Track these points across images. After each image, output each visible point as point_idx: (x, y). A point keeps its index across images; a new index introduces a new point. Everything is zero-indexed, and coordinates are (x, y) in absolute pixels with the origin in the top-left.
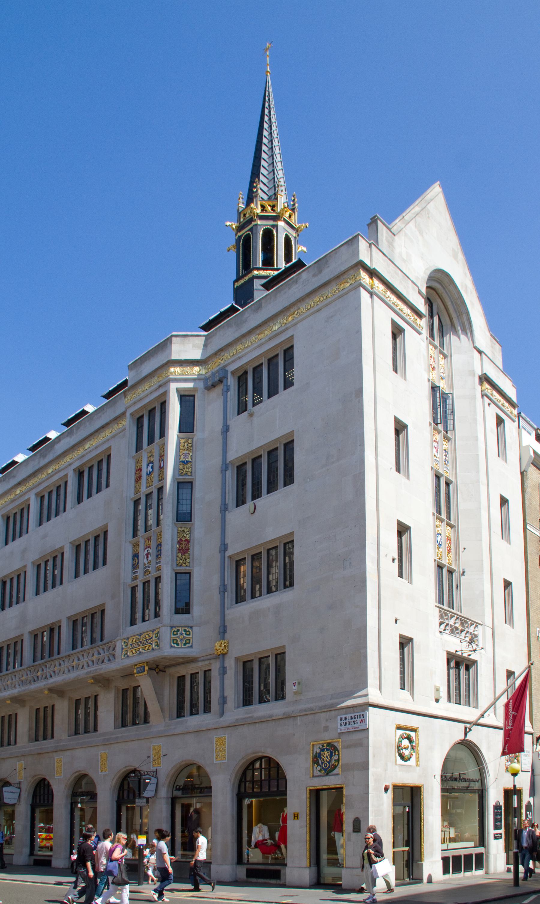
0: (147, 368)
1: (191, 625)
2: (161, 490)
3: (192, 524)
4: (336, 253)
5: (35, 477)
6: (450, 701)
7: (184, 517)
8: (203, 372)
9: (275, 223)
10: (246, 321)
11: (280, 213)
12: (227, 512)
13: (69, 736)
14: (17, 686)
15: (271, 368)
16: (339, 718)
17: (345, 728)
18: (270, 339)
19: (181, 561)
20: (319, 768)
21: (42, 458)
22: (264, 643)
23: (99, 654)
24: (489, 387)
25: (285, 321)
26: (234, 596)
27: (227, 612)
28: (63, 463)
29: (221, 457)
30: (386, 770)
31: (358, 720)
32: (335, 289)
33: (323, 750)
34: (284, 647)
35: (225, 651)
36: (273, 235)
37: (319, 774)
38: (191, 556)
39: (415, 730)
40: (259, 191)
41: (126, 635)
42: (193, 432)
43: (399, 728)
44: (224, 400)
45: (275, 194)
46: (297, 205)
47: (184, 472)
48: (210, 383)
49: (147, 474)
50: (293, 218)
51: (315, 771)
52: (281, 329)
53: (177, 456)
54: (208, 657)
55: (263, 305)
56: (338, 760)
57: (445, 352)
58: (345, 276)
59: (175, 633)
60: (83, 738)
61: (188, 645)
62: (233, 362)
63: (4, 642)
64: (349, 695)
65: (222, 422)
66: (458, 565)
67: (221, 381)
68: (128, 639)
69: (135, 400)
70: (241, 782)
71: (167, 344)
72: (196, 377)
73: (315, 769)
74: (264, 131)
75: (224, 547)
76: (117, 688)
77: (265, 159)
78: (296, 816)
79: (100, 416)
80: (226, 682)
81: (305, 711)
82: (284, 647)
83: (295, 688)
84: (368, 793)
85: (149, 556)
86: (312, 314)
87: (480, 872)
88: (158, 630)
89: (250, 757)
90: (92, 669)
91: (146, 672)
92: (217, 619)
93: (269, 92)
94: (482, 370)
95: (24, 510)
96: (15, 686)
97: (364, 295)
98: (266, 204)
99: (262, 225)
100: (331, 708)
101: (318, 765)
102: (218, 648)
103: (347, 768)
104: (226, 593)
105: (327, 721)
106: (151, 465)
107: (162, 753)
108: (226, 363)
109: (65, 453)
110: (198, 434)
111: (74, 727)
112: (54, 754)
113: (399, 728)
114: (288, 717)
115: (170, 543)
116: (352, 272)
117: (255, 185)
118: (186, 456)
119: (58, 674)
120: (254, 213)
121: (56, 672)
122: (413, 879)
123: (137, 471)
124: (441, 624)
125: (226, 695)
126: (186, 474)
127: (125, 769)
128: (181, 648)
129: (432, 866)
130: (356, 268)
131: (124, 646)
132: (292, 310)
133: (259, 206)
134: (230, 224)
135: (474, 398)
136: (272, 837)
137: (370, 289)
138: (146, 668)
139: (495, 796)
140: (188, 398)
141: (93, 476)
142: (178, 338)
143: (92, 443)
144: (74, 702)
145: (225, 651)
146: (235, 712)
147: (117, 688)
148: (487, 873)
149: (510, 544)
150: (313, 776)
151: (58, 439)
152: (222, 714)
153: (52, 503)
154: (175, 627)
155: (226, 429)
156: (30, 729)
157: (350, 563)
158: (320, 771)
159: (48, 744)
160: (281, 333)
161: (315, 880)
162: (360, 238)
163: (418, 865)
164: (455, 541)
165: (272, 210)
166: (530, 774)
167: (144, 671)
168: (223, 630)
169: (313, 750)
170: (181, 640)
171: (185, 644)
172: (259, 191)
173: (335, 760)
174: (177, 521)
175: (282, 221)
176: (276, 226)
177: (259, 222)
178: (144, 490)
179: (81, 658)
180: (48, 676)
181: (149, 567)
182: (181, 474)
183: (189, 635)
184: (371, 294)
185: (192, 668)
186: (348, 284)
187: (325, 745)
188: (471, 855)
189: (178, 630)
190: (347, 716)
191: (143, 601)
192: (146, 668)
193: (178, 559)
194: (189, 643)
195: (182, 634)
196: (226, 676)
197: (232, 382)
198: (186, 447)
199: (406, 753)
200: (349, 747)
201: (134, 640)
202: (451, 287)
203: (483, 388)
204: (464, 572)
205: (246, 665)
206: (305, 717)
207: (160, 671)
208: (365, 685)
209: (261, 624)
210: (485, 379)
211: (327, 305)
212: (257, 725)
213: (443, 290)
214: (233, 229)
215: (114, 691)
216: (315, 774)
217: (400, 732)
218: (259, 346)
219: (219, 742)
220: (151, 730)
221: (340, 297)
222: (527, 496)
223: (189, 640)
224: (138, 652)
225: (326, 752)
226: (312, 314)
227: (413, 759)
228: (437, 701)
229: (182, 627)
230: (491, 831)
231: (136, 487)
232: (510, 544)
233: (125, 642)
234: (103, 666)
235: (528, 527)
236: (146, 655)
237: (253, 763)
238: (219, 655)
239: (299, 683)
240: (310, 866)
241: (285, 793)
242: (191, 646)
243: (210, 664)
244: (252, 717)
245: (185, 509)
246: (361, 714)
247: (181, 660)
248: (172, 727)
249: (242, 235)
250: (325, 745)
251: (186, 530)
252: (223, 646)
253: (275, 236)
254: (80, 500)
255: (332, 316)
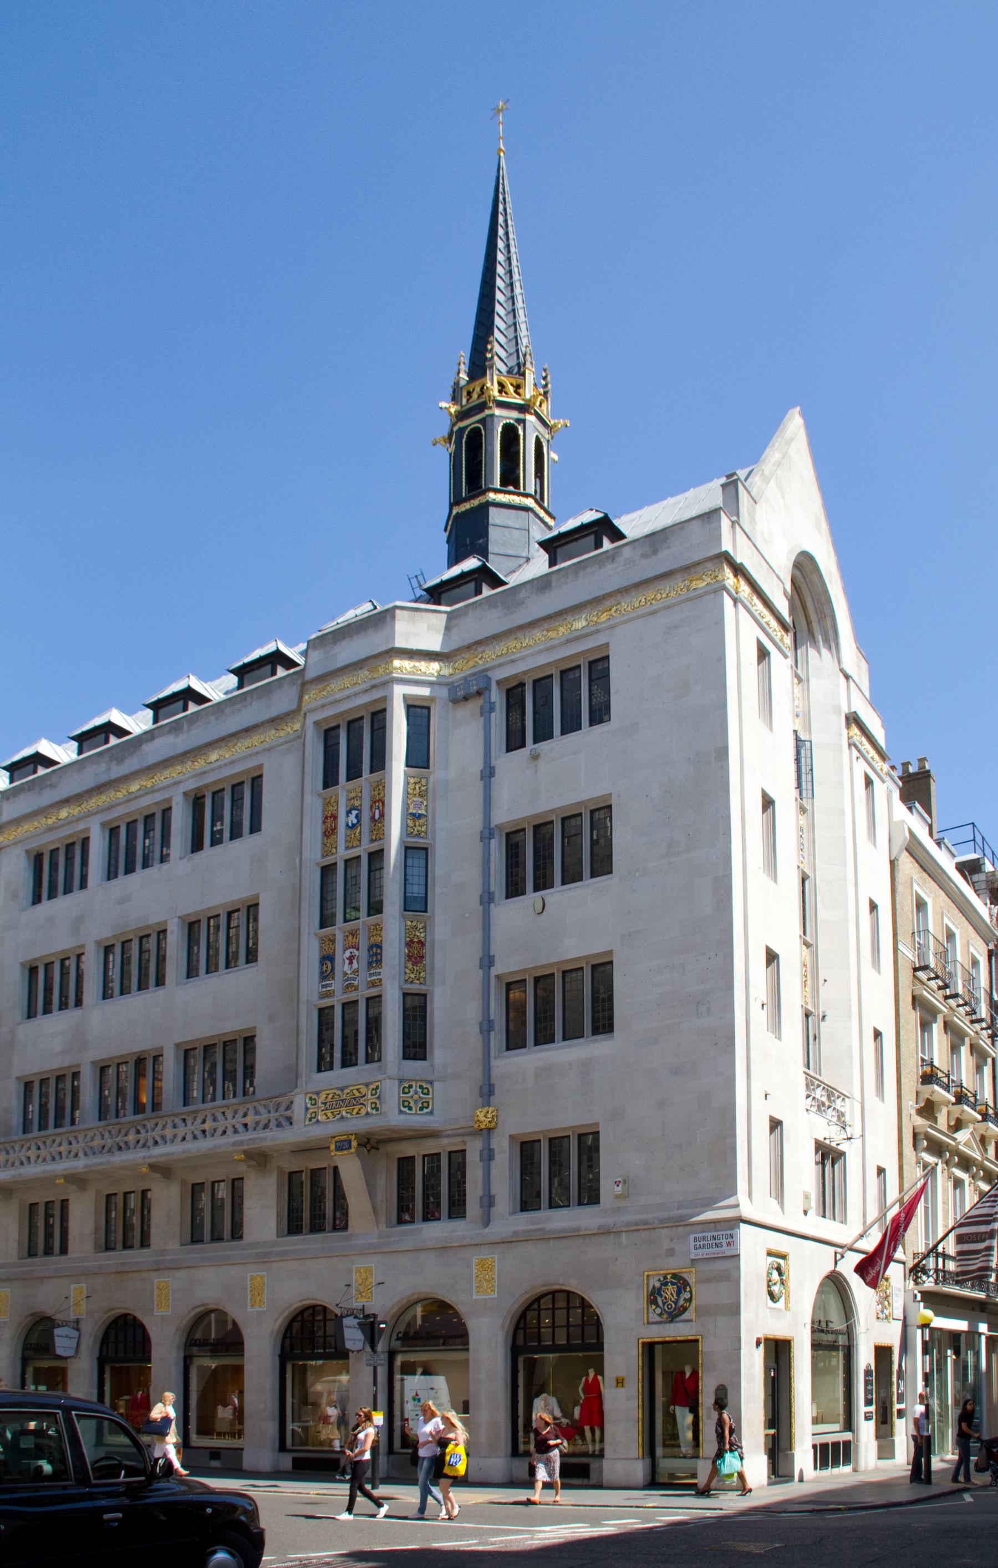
0: (348, 652)
1: (431, 1078)
2: (377, 857)
3: (430, 917)
4: (682, 529)
5: (101, 793)
6: (824, 1216)
7: (416, 904)
8: (446, 671)
9: (521, 416)
10: (523, 603)
11: (530, 400)
12: (492, 905)
13: (182, 1245)
14: (81, 1154)
15: (565, 685)
16: (692, 1237)
17: (702, 1253)
18: (568, 641)
19: (413, 976)
20: (658, 1311)
21: (114, 763)
22: (566, 1117)
23: (257, 1113)
24: (859, 733)
25: (595, 619)
26: (504, 1038)
27: (494, 1063)
28: (162, 778)
29: (481, 816)
30: (757, 1316)
31: (724, 1242)
32: (681, 585)
33: (666, 1284)
34: (597, 1124)
35: (493, 1124)
36: (518, 436)
37: (658, 1319)
38: (428, 968)
39: (784, 1257)
40: (496, 358)
41: (313, 1087)
42: (428, 767)
43: (770, 1254)
44: (485, 725)
45: (519, 365)
46: (550, 386)
47: (415, 832)
48: (461, 693)
49: (347, 825)
50: (544, 406)
51: (651, 1315)
52: (588, 630)
53: (406, 806)
54: (459, 1131)
55: (554, 584)
56: (690, 1300)
57: (799, 672)
58: (699, 569)
59: (406, 1090)
60: (210, 1249)
61: (425, 1110)
62: (500, 665)
63: (34, 1074)
64: (709, 1203)
65: (482, 759)
66: (816, 1005)
67: (479, 693)
68: (318, 1093)
69: (323, 701)
70: (517, 1328)
71: (385, 618)
72: (434, 679)
73: (651, 1310)
74: (499, 253)
75: (487, 961)
76: (280, 1170)
77: (501, 301)
78: (620, 1382)
79: (240, 710)
80: (494, 1172)
81: (637, 1224)
82: (597, 1124)
83: (618, 1190)
84: (739, 1349)
85: (355, 961)
86: (642, 616)
87: (846, 1469)
88: (378, 1083)
89: (538, 1291)
90: (250, 1135)
91: (353, 1150)
92: (478, 1072)
93: (503, 185)
94: (849, 707)
95: (77, 848)
96: (76, 1155)
97: (728, 602)
98: (507, 382)
99: (502, 417)
100: (679, 1222)
101: (657, 1305)
102: (482, 1118)
103: (704, 1311)
104: (492, 1034)
105: (671, 1240)
106: (354, 812)
107: (373, 1280)
108: (488, 665)
109: (166, 763)
110: (437, 773)
111: (189, 1230)
112: (153, 1274)
113: (770, 1254)
114: (606, 1232)
115: (396, 945)
116: (709, 565)
117: (489, 347)
118: (418, 805)
119: (173, 1141)
120: (489, 397)
121: (168, 1138)
122: (779, 1476)
123: (326, 818)
124: (808, 1096)
125: (493, 1192)
126: (418, 835)
127: (300, 1304)
128: (416, 1114)
129: (803, 1457)
130: (717, 561)
131: (309, 1105)
132: (608, 603)
133: (496, 385)
134: (447, 405)
135: (841, 749)
136: (567, 1413)
137: (734, 593)
138: (354, 1144)
139: (865, 1358)
140: (419, 710)
141: (228, 810)
142: (405, 612)
143: (221, 753)
144: (190, 1188)
145: (493, 1124)
146: (508, 1220)
147: (280, 1170)
148: (855, 1470)
149: (879, 972)
150: (648, 1323)
151: (148, 736)
152: (487, 1222)
153: (135, 845)
154: (405, 1080)
155: (488, 773)
156: (97, 1229)
157: (709, 1008)
158: (660, 1315)
159: (136, 1256)
160: (587, 635)
161: (649, 1478)
162: (722, 513)
163: (787, 1456)
164: (812, 967)
165: (516, 392)
166: (900, 1323)
167: (350, 1148)
168: (487, 1091)
169: (648, 1284)
170: (416, 1102)
171: (421, 1109)
172: (496, 358)
173: (686, 1300)
174: (405, 910)
175: (531, 414)
176: (523, 422)
177: (497, 412)
178: (342, 853)
179: (220, 1117)
180: (151, 1142)
181: (354, 979)
182: (410, 835)
183: (428, 1094)
184: (735, 601)
185: (430, 1147)
186: (705, 584)
187: (669, 1277)
188: (838, 1443)
189: (411, 1086)
190: (706, 1234)
191: (345, 1037)
192: (354, 1144)
193: (408, 971)
194: (427, 1108)
195: (416, 1093)
196: (493, 1163)
197: (497, 697)
198: (418, 791)
199: (776, 1289)
200: (708, 1280)
201: (330, 1096)
202: (815, 578)
203: (851, 734)
204: (824, 1017)
205: (527, 1150)
206: (635, 1233)
207: (372, 1147)
208: (733, 1191)
209: (552, 1085)
210: (853, 720)
211: (667, 608)
212: (552, 1242)
213: (802, 580)
214: (451, 414)
215: (275, 1175)
216: (651, 1320)
217: (771, 1259)
218: (550, 649)
219: (484, 1266)
220: (353, 1242)
221: (688, 600)
222: (898, 899)
223: (428, 1102)
224: (338, 1117)
225: (670, 1287)
226: (642, 616)
227: (782, 1300)
228: (805, 1213)
229: (416, 1081)
230: (861, 1408)
231: (324, 844)
232: (879, 972)
233: (311, 1099)
234: (267, 1134)
235: (900, 947)
236: (354, 1122)
237: (538, 1299)
238: (481, 1130)
239: (625, 1182)
240: (643, 1457)
241: (600, 1346)
242: (431, 1113)
243: (465, 1143)
244: (542, 1229)
245: (416, 890)
246: (729, 1232)
247: (411, 1133)
248: (393, 1239)
249: (466, 427)
250: (669, 1277)
251: (420, 926)
252: (489, 1116)
253: (522, 437)
254: (197, 845)
255: (676, 627)
